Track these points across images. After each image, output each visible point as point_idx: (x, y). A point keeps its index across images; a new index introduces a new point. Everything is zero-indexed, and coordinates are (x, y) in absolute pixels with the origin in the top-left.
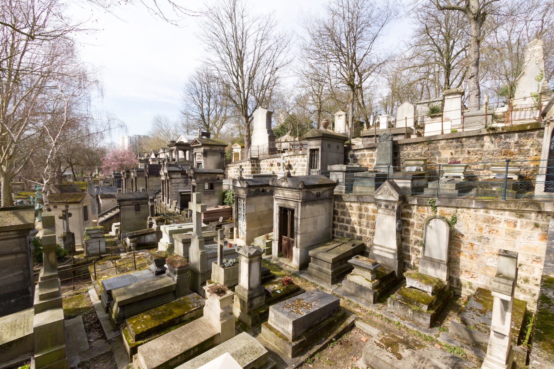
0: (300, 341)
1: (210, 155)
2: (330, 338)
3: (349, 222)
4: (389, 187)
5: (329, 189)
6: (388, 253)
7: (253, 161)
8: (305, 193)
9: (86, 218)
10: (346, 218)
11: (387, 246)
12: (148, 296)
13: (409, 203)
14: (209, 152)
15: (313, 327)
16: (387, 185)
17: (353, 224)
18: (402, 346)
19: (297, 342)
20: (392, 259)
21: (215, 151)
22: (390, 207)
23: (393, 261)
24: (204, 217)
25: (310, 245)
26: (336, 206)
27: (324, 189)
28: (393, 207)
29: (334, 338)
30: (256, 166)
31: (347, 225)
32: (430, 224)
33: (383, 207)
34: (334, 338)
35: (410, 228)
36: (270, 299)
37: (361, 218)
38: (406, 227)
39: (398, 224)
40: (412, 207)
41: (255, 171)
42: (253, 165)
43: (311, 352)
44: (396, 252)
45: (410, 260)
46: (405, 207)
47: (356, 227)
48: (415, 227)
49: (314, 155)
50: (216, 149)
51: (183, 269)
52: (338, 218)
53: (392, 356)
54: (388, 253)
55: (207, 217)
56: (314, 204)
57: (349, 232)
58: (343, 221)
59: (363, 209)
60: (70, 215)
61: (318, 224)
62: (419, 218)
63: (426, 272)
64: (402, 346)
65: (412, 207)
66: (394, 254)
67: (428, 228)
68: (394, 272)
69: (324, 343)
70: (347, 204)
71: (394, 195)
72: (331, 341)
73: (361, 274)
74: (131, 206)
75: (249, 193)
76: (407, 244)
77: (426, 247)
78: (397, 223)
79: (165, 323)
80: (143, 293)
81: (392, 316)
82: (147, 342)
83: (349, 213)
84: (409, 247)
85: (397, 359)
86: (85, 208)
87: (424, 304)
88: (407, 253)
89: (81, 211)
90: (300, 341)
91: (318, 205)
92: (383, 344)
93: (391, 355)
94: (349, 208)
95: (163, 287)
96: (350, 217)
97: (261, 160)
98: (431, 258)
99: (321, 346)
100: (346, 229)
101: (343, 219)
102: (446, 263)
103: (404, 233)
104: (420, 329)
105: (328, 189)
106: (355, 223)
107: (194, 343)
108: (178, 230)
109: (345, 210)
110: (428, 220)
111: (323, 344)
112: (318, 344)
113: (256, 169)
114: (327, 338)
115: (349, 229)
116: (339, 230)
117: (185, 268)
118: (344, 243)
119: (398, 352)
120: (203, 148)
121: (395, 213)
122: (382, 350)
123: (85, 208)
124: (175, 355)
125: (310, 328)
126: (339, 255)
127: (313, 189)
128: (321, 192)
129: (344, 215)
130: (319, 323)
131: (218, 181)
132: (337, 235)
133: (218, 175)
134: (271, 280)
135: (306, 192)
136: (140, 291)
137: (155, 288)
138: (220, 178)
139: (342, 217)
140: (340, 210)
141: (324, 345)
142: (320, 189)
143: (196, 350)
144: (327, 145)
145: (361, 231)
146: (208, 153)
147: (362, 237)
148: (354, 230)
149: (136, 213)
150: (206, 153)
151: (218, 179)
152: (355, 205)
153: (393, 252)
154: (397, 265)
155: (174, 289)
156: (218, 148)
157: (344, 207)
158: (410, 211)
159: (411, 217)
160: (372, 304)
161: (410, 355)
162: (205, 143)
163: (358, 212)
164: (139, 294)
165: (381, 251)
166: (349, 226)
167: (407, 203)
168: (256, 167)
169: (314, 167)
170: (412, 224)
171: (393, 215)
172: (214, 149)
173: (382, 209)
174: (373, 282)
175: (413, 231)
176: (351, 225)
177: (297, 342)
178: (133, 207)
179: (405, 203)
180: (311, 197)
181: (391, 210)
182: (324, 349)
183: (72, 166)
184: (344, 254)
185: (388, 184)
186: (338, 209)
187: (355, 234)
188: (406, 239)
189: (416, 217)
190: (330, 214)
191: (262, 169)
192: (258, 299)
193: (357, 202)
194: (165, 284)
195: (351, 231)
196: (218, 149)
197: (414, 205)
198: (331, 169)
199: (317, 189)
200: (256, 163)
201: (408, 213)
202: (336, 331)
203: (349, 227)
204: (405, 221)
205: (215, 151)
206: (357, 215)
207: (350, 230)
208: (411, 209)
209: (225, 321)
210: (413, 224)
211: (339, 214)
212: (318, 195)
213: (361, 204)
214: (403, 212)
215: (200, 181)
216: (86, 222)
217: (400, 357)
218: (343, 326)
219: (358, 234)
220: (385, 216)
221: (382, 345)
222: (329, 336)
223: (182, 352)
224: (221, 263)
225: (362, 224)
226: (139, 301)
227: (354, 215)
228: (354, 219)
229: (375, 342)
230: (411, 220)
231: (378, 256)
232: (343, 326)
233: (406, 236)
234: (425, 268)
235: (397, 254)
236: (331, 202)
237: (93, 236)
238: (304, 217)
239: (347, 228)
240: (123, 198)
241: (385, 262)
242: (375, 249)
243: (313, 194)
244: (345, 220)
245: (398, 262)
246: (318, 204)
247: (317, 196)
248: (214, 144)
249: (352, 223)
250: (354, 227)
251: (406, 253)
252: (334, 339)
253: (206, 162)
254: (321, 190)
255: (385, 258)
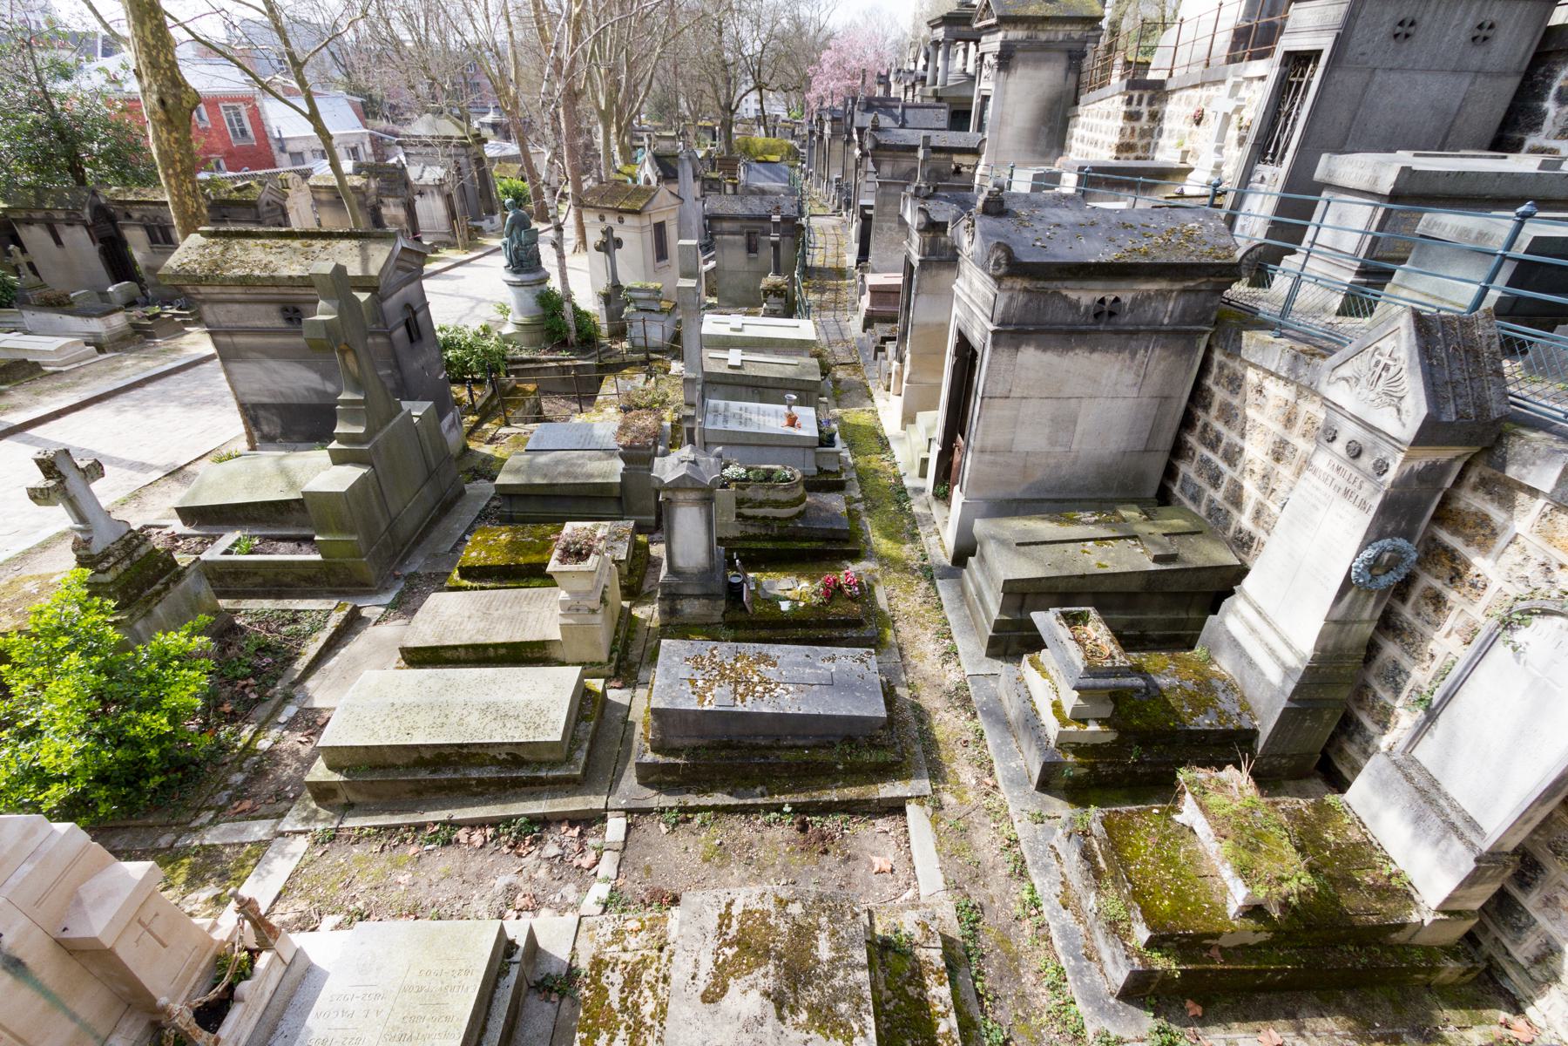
0: (672, 760)
1: (1025, 62)
2: (777, 799)
3: (1232, 456)
4: (1403, 354)
5: (1184, 291)
6: (1272, 652)
7: (1136, 94)
8: (1021, 298)
9: (661, 252)
10: (1229, 436)
11: (1283, 625)
12: (558, 491)
13: (1512, 472)
14: (1024, 50)
15: (738, 748)
16: (1397, 338)
17: (1242, 473)
18: (765, 975)
19: (660, 759)
20: (1270, 684)
21: (1046, 47)
22: (1366, 462)
23: (1268, 694)
24: (872, 303)
25: (1018, 496)
26: (1215, 370)
27: (1152, 287)
28: (1381, 468)
29: (791, 804)
30: (1145, 117)
31: (1223, 466)
32: (1521, 636)
33: (1339, 446)
34: (791, 804)
35: (1452, 596)
36: (740, 616)
37: (1278, 460)
38: (1438, 584)
39: (1369, 553)
40: (1522, 497)
41: (1135, 140)
42: (1131, 116)
43: (692, 800)
44: (1302, 668)
45: (1384, 726)
46: (1485, 485)
47: (1251, 491)
48: (1482, 604)
49: (1299, 84)
50: (1052, 37)
51: (634, 452)
52: (1206, 425)
53: (702, 975)
54: (1272, 652)
55: (881, 304)
56: (1073, 349)
57: (1219, 496)
58: (1213, 445)
59: (1300, 422)
60: (619, 243)
61: (1079, 429)
62: (1527, 572)
63: (1375, 818)
64: (765, 975)
65: (1522, 497)
66: (1287, 671)
67: (1500, 652)
68: (1253, 734)
69: (749, 801)
70: (1252, 376)
71: (1407, 404)
72: (778, 808)
73: (1055, 678)
74: (737, 237)
75: (933, 252)
76: (1405, 662)
77: (1443, 720)
78: (1365, 545)
79: (518, 565)
80: (545, 482)
81: (1046, 867)
82: (476, 589)
83: (1245, 418)
84: (1408, 675)
85: (699, 994)
86: (660, 228)
87: (1146, 920)
88: (1386, 696)
89: (649, 236)
90: (672, 760)
91: (1096, 356)
92: (735, 925)
93: (707, 964)
94: (1251, 396)
95: (591, 481)
96: (1243, 436)
97: (1173, 91)
98: (1434, 783)
99: (733, 801)
100: (1215, 479)
101: (1218, 439)
102: (1485, 846)
103: (1416, 605)
104: (1079, 973)
105: (1178, 286)
106: (1252, 471)
107: (502, 634)
108: (728, 337)
109: (1236, 402)
110: (1522, 605)
111: (741, 802)
112: (730, 794)
113: (1144, 133)
114: (771, 795)
115: (1224, 486)
116: (1193, 475)
117: (640, 452)
118: (1134, 537)
119: (731, 981)
120: (1000, 36)
121: (1375, 502)
122: (710, 937)
123: (660, 228)
124: (457, 643)
125: (728, 746)
126: (1053, 573)
127: (1068, 284)
128: (1127, 298)
129: (1227, 423)
130: (769, 748)
131: (956, 181)
132: (1182, 489)
133: (957, 159)
134: (842, 559)
135: (1026, 290)
136: (545, 476)
137: (576, 478)
138: (964, 169)
139: (1219, 426)
140: (1220, 394)
141: (744, 805)
142: (1123, 285)
143: (502, 651)
144: (1387, 26)
145: (1258, 514)
146: (1019, 55)
147: (1252, 539)
148: (1236, 499)
149: (749, 259)
150: (1010, 57)
151: (958, 171)
152: (1277, 392)
153: (1292, 661)
154: (1276, 717)
155: (616, 492)
156: (1060, 33)
157: (1236, 383)
158: (1497, 514)
159: (1484, 547)
160: (1032, 787)
161: (744, 1016)
162: (1012, 12)
163: (1277, 428)
164: (538, 480)
165: (1253, 630)
166: (1228, 473)
167: (1502, 467)
168: (1144, 122)
169: (1274, 155)
170: (1473, 585)
171: (1363, 506)
172: (1043, 37)
173: (1333, 453)
174: (1073, 728)
175: (1463, 618)
176: (1235, 475)
177: (660, 759)
178: (741, 239)
179: (1490, 464)
180: (1056, 314)
181: (1368, 477)
182: (742, 813)
183: (760, 90)
184: (1083, 576)
185: (1404, 333)
186: (1214, 388)
187: (1234, 512)
188: (1412, 634)
189: (1513, 556)
190: (1164, 399)
191: (1165, 134)
192: (696, 602)
193: (1287, 381)
194: (599, 476)
195: (1226, 498)
196: (1061, 37)
197: (1533, 492)
198: (1330, 173)
199: (1099, 285)
200: (1150, 103)
201: (1484, 520)
202: (814, 794)
203: (1226, 479)
204: (1452, 555)
205: (1046, 47)
206: (1270, 439)
207: (1227, 490)
208: (1507, 502)
209: (570, 621)
210: (1479, 586)
211: (1214, 411)
212: (1105, 312)
213: (1299, 395)
214: (1462, 505)
215: (892, 177)
216: (662, 263)
217: (711, 997)
218: (851, 793)
219: (1245, 520)
220: (1330, 491)
221: (729, 927)
222: (779, 794)
223: (469, 642)
224: (72, 529)
225: (1273, 485)
226: (543, 496)
227: (1260, 437)
228: (1255, 450)
229: (729, 905)
230: (1480, 563)
231: (1235, 644)
232: (851, 793)
233: (1418, 623)
234: (1377, 801)
235: (1297, 678)
236: (1190, 348)
237: (641, 305)
238: (1000, 390)
239: (1218, 478)
240: (720, 212)
241: (1242, 679)
242: (1236, 613)
243: (1075, 306)
244: (1224, 441)
245: (1286, 710)
246: (1093, 350)
247: (1096, 316)
248: (1055, 13)
249: (1239, 468)
250: (1241, 487)
251: (1380, 693)
252: (787, 809)
253: (1005, 92)
254: (1126, 292)
255: (1251, 663)
